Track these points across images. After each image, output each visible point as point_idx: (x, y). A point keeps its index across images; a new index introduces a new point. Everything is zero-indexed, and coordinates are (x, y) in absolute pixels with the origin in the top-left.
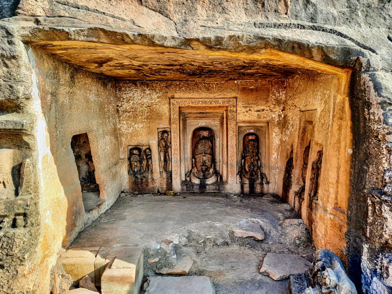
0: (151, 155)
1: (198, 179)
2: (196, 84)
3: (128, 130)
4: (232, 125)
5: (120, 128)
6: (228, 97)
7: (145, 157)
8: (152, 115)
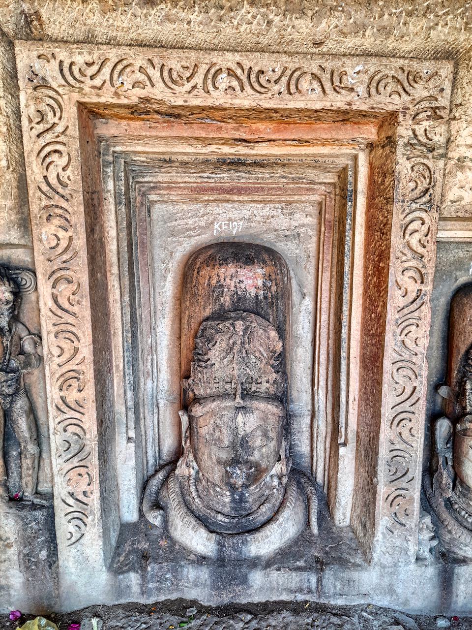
4: (417, 236)
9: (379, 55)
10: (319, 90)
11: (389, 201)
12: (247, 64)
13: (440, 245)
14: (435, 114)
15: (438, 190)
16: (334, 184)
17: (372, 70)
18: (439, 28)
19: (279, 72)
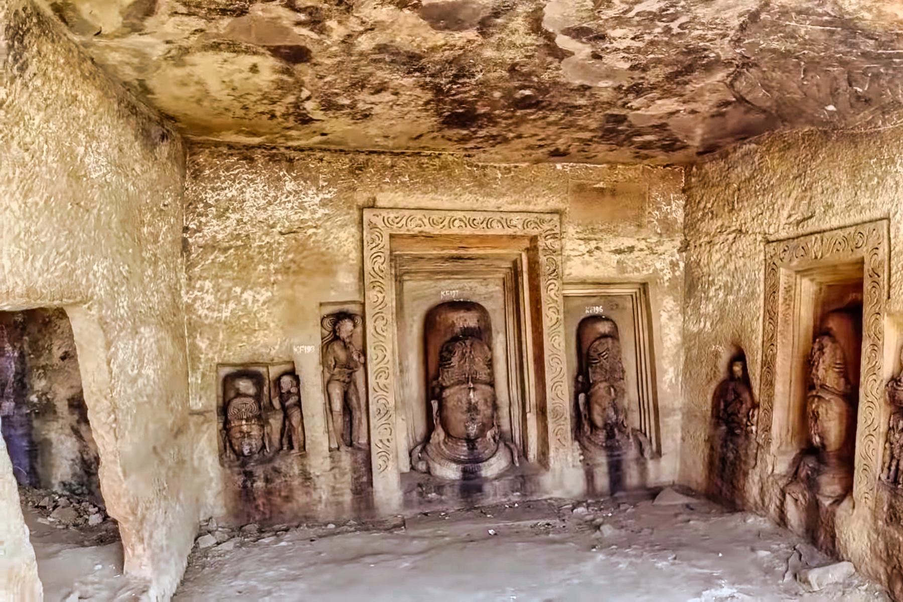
0: (298, 394)
1: (454, 466)
2: (444, 167)
3: (219, 311)
5: (192, 305)
6: (537, 209)
7: (276, 403)
8: (304, 260)
10: (501, 227)
11: (538, 275)
13: (566, 297)
14: (554, 237)
15: (560, 269)
16: (510, 268)
19: (482, 219)
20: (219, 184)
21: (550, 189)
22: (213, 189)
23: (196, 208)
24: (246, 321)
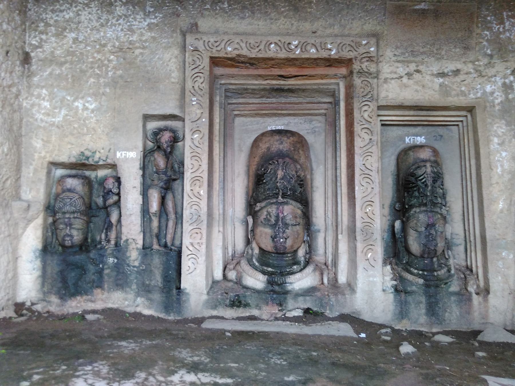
0: (119, 194)
9: (342, 36)
12: (283, 41)
14: (370, 59)
17: (339, 42)
18: (367, 24)
20: (58, 7)
21: (367, 11)
22: (53, 11)
23: (38, 26)
24: (76, 126)
